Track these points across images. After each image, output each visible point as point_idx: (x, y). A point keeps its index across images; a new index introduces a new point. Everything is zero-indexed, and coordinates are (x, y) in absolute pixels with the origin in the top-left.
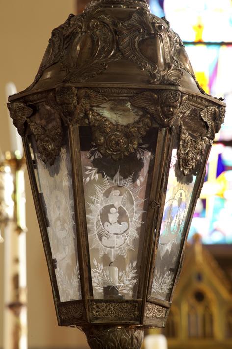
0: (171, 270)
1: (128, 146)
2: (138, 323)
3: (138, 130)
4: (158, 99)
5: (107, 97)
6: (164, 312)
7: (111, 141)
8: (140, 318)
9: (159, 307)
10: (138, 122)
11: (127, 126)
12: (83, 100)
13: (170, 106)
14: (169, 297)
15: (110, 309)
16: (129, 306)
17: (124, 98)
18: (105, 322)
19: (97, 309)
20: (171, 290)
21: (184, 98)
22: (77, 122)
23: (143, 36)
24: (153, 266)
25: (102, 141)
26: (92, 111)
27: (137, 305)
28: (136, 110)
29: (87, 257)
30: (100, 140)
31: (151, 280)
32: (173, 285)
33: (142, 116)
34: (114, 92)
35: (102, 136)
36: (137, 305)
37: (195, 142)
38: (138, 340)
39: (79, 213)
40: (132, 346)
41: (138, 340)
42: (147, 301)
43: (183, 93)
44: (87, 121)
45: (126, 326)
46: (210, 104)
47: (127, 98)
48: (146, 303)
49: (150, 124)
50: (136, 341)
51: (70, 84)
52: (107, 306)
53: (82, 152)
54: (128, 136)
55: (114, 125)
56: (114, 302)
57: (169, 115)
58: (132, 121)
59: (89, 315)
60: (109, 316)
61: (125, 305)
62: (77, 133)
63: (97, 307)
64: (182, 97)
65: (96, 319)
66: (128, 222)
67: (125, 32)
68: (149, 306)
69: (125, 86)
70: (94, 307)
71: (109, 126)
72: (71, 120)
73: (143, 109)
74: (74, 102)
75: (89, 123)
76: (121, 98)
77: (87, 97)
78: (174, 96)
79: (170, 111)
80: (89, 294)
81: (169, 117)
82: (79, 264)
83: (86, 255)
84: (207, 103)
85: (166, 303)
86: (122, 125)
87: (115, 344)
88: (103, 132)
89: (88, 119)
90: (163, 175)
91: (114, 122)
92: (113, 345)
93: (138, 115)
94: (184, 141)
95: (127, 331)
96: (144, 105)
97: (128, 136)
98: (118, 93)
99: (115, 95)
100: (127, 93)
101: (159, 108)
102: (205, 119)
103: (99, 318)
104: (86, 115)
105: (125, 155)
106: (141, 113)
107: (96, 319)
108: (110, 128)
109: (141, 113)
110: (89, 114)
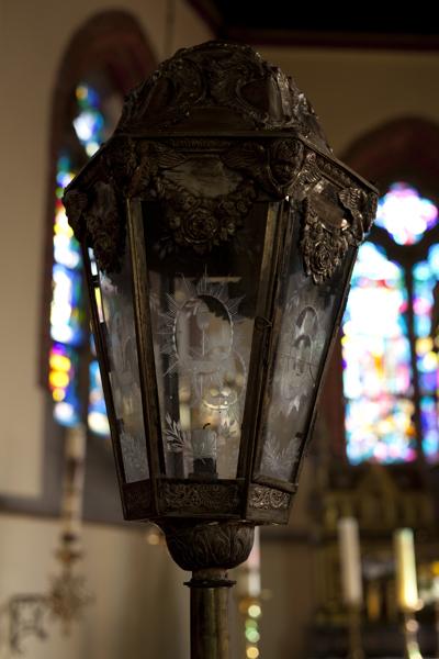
0: (298, 435)
1: (219, 231)
2: (239, 516)
3: (235, 205)
4: (266, 153)
5: (184, 153)
6: (286, 499)
7: (191, 223)
8: (241, 509)
9: (276, 491)
10: (234, 193)
11: (217, 200)
12: (145, 159)
13: (285, 163)
14: (294, 477)
15: (192, 494)
16: (224, 489)
17: (213, 156)
18: (184, 514)
19: (172, 494)
20: (296, 466)
21: (308, 156)
22: (137, 194)
23: (248, 79)
24: (262, 426)
25: (178, 223)
26: (162, 177)
27: (237, 488)
28: (231, 174)
29: (155, 411)
30: (173, 222)
31: (259, 447)
32: (299, 457)
33: (242, 183)
34: (196, 146)
35: (178, 215)
36: (237, 488)
37: (331, 235)
38: (242, 543)
39: (213, 600)
40: (232, 552)
41: (242, 543)
42: (253, 482)
43: (306, 146)
44: (154, 193)
45: (223, 521)
46: (354, 184)
47: (217, 156)
48: (251, 485)
49: (254, 195)
50: (239, 545)
51: (124, 134)
52: (187, 489)
53: (151, 273)
54: (220, 215)
55: (196, 198)
56: (199, 483)
57: (284, 179)
58: (225, 191)
59: (159, 503)
60: (191, 505)
61: (216, 488)
62: (138, 211)
63: (171, 490)
64: (305, 153)
65: (171, 509)
66: (225, 376)
67: (221, 72)
68: (259, 490)
69: (213, 134)
70: (168, 490)
71: (188, 199)
72: (127, 191)
73: (246, 174)
74: (131, 161)
75: (158, 194)
76: (207, 156)
77: (153, 153)
78: (292, 146)
79: (284, 170)
80: (159, 469)
81: (283, 183)
82: (88, 254)
83: (152, 407)
84: (348, 180)
85: (289, 486)
86: (209, 199)
87: (204, 550)
88: (179, 210)
89: (156, 189)
90: (277, 276)
91: (197, 194)
92: (200, 550)
93: (234, 182)
94: (312, 226)
95: (225, 531)
96: (243, 165)
97: (220, 215)
98: (203, 148)
99: (197, 150)
100: (216, 147)
101: (268, 168)
102: (347, 206)
103: (175, 509)
104: (152, 185)
105: (214, 247)
106: (240, 179)
107: (171, 509)
108: (190, 203)
109: (240, 179)
110: (156, 181)
